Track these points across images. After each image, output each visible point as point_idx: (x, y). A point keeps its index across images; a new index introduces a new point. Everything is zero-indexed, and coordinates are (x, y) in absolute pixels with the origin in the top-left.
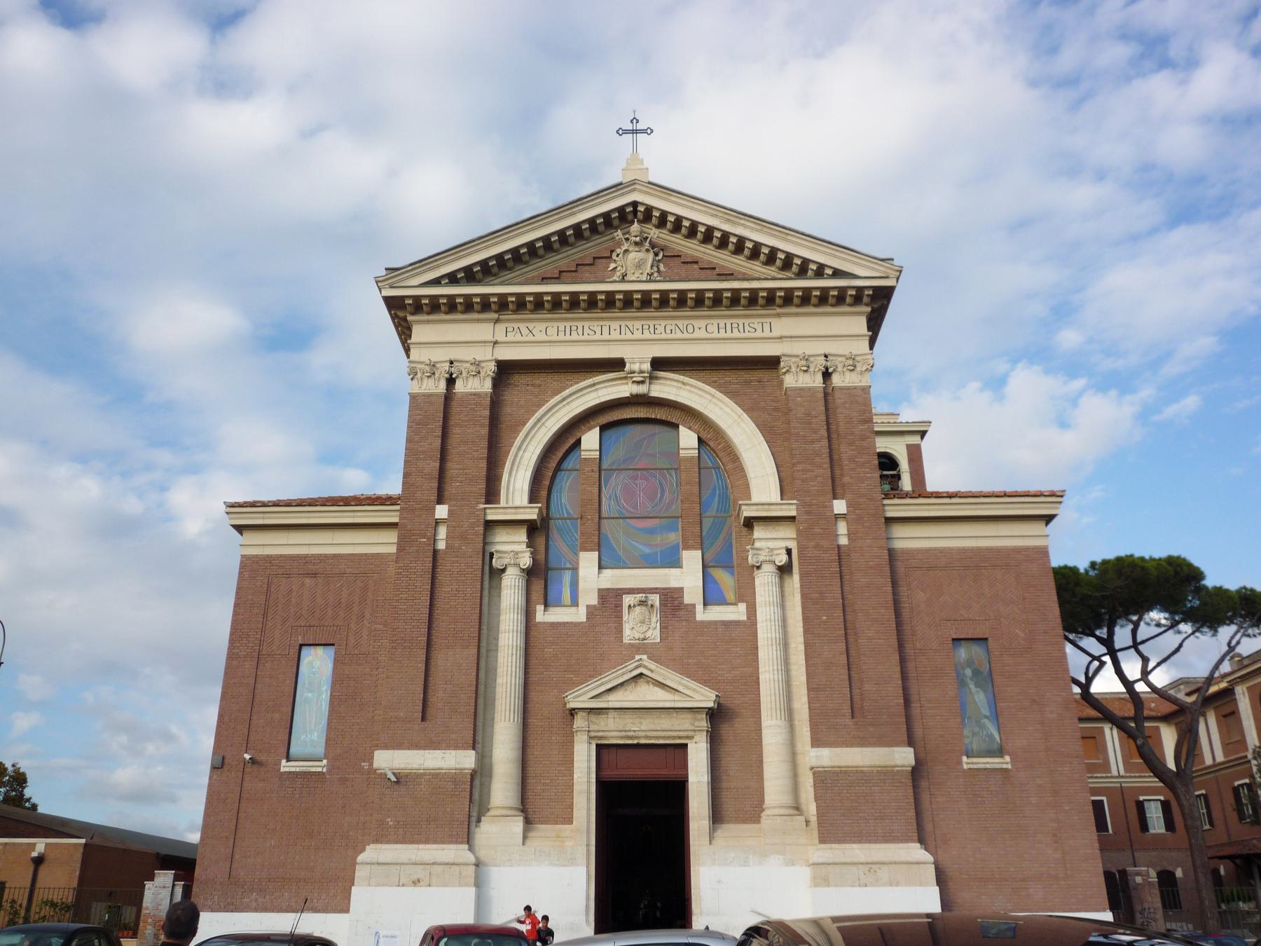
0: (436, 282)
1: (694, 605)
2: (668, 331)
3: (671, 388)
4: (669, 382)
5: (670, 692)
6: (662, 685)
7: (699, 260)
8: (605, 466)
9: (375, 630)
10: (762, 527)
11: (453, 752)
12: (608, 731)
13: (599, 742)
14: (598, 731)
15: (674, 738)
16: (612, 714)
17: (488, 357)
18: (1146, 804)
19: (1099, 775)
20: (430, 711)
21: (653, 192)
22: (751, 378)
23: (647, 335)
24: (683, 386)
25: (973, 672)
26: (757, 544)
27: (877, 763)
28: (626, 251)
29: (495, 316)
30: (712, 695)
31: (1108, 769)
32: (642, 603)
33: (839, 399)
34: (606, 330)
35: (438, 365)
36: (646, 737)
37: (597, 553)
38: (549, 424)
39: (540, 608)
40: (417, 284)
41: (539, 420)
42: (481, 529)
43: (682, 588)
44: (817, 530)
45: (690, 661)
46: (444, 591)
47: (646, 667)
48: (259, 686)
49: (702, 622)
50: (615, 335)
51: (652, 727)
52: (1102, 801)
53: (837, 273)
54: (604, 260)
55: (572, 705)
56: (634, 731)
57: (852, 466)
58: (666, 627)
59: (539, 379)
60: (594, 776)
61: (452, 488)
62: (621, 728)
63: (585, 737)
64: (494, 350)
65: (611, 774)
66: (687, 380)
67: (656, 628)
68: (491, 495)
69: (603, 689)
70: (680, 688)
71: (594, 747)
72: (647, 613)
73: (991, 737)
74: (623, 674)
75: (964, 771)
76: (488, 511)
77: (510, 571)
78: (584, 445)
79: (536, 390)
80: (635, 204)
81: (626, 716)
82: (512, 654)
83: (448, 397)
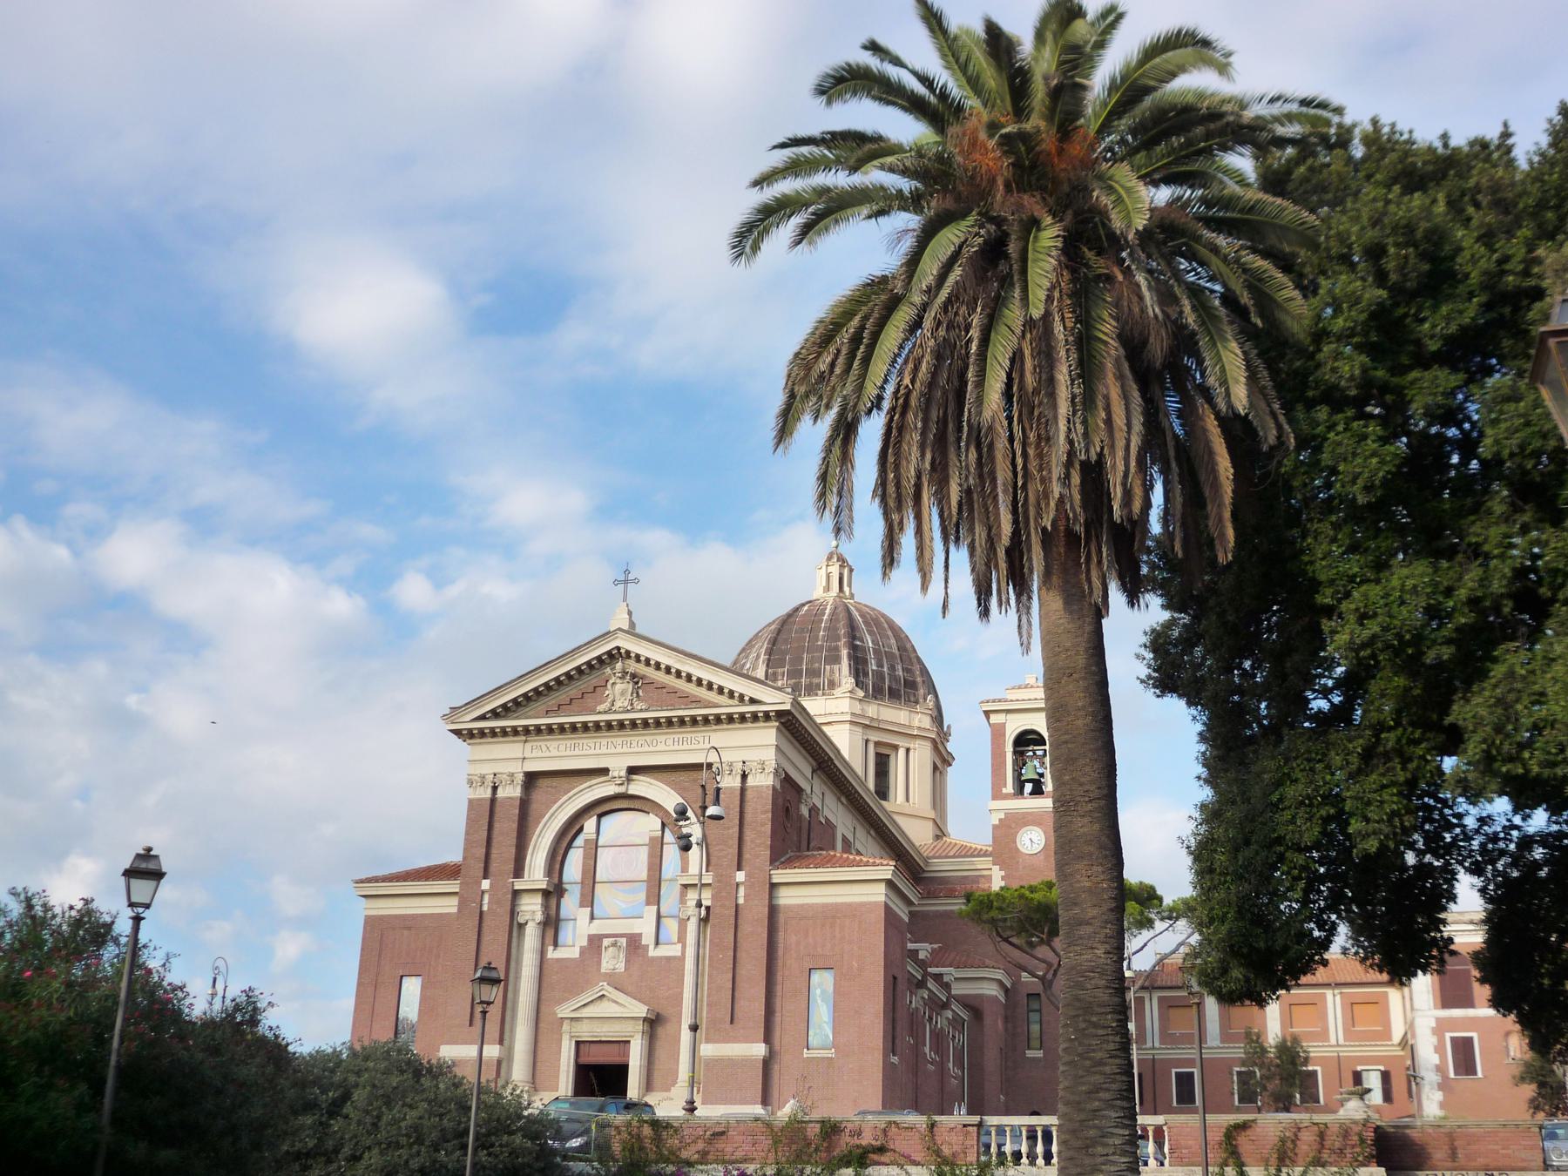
0: (483, 718)
3: (642, 787)
17: (518, 769)
18: (1364, 1074)
19: (1315, 1044)
23: (625, 749)
29: (524, 738)
30: (645, 1009)
31: (1327, 1038)
32: (614, 945)
33: (749, 795)
39: (551, 948)
41: (553, 815)
42: (510, 896)
44: (724, 894)
46: (486, 939)
49: (652, 957)
50: (604, 750)
52: (1316, 1072)
53: (753, 701)
55: (560, 1016)
59: (555, 782)
60: (572, 1061)
61: (493, 867)
65: (584, 1060)
66: (652, 781)
68: (518, 872)
69: (583, 1003)
73: (827, 1036)
77: (530, 924)
79: (553, 790)
80: (618, 648)
83: (493, 800)
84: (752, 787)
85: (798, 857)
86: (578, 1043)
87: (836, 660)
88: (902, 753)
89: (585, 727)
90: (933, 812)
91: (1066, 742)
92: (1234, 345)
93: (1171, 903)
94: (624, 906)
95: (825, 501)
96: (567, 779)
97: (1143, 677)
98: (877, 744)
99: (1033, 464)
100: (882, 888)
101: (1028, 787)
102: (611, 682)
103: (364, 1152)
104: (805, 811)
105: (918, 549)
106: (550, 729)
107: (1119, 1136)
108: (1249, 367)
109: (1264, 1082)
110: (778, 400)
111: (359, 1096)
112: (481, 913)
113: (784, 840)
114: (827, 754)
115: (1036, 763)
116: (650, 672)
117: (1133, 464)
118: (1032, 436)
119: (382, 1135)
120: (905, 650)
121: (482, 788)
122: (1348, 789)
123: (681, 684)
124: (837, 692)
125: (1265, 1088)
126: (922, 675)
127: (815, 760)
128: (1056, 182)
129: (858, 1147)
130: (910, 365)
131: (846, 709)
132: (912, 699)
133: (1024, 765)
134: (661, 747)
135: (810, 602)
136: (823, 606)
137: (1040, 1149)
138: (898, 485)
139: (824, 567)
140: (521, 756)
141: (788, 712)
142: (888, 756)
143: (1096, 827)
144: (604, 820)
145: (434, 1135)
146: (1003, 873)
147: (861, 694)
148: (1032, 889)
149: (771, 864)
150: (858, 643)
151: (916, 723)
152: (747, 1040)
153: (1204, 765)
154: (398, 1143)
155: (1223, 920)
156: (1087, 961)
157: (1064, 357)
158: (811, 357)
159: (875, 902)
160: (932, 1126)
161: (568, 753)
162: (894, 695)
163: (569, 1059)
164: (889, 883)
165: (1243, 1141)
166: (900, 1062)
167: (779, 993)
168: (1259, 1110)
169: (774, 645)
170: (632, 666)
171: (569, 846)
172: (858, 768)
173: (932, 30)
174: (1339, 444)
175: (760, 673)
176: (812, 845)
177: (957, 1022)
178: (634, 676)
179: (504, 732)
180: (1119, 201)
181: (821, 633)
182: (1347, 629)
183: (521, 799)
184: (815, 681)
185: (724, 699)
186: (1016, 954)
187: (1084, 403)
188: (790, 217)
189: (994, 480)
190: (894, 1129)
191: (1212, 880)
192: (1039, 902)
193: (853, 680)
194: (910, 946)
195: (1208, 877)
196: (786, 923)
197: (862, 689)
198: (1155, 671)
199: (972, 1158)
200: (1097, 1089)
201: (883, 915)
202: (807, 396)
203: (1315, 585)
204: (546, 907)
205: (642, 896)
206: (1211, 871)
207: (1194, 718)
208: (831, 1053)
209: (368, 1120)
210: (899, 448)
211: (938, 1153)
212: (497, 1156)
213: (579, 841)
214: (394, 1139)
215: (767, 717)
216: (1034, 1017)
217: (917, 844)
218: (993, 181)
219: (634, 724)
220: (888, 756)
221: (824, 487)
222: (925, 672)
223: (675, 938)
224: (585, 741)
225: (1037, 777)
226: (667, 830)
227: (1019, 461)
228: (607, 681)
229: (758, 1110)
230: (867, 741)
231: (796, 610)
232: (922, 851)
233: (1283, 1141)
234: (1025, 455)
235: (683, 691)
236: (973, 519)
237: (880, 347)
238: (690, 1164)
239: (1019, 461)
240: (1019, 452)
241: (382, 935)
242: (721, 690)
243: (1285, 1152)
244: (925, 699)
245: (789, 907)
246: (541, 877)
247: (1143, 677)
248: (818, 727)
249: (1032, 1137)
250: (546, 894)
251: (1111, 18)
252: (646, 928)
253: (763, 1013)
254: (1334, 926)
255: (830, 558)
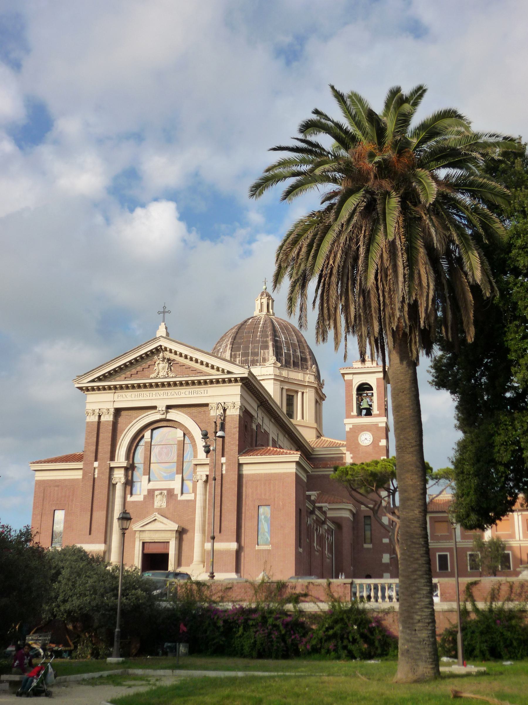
0: (93, 381)
3: (173, 415)
8: (153, 444)
20: (92, 532)
23: (165, 397)
26: (198, 473)
29: (114, 391)
30: (177, 526)
31: (515, 538)
32: (161, 494)
33: (227, 419)
39: (129, 496)
41: (129, 430)
42: (108, 470)
48: (42, 524)
50: (154, 397)
52: (446, 556)
53: (229, 372)
55: (134, 529)
61: (100, 456)
65: (146, 551)
68: (112, 458)
73: (267, 539)
80: (161, 346)
83: (99, 422)
87: (266, 347)
88: (300, 394)
91: (401, 421)
92: (475, 252)
93: (437, 471)
95: (291, 310)
96: (138, 411)
97: (430, 381)
98: (287, 390)
99: (387, 301)
100: (294, 465)
101: (364, 412)
102: (157, 363)
103: (69, 598)
104: (254, 427)
107: (425, 590)
108: (482, 263)
109: (483, 559)
110: (273, 268)
111: (65, 573)
114: (265, 398)
115: (368, 400)
116: (177, 358)
117: (430, 303)
118: (387, 289)
119: (77, 590)
120: (301, 342)
122: (523, 438)
123: (193, 364)
124: (267, 364)
125: (483, 562)
126: (310, 355)
128: (396, 173)
129: (294, 594)
130: (333, 255)
131: (272, 373)
132: (305, 367)
133: (362, 400)
134: (183, 395)
135: (253, 317)
136: (259, 319)
137: (380, 594)
138: (329, 309)
139: (259, 300)
142: (293, 396)
143: (415, 458)
144: (155, 432)
145: (102, 590)
146: (352, 455)
147: (279, 365)
148: (368, 465)
151: (307, 380)
152: (228, 540)
153: (458, 420)
155: (468, 495)
156: (411, 516)
157: (401, 256)
160: (329, 584)
161: (136, 398)
162: (295, 365)
165: (475, 591)
166: (303, 551)
168: (481, 575)
169: (234, 339)
170: (168, 355)
171: (137, 445)
173: (339, 101)
174: (519, 292)
176: (258, 443)
177: (329, 531)
178: (169, 360)
179: (104, 388)
180: (424, 188)
182: (522, 372)
183: (113, 422)
184: (256, 358)
185: (214, 372)
186: (358, 496)
187: (409, 278)
188: (277, 182)
189: (370, 307)
190: (311, 585)
191: (463, 477)
192: (371, 472)
193: (275, 358)
194: (308, 493)
195: (461, 475)
196: (246, 483)
197: (279, 362)
198: (436, 378)
199: (348, 598)
200: (415, 570)
202: (287, 267)
203: (508, 351)
204: (126, 475)
206: (462, 472)
207: (454, 400)
208: (269, 547)
209: (70, 583)
210: (329, 293)
211: (332, 596)
212: (130, 600)
213: (142, 443)
214: (83, 592)
215: (236, 380)
216: (368, 527)
217: (308, 441)
218: (368, 173)
219: (169, 384)
220: (293, 396)
221: (291, 303)
223: (191, 491)
224: (145, 393)
225: (368, 407)
226: (186, 437)
227: (381, 299)
230: (282, 389)
231: (246, 322)
233: (493, 590)
234: (384, 296)
235: (193, 367)
236: (361, 324)
239: (381, 299)
240: (381, 295)
241: (44, 490)
242: (213, 367)
243: (494, 595)
244: (311, 367)
245: (248, 475)
247: (430, 381)
248: (258, 381)
249: (376, 587)
250: (126, 469)
251: (420, 92)
252: (176, 485)
254: (516, 495)
255: (262, 295)
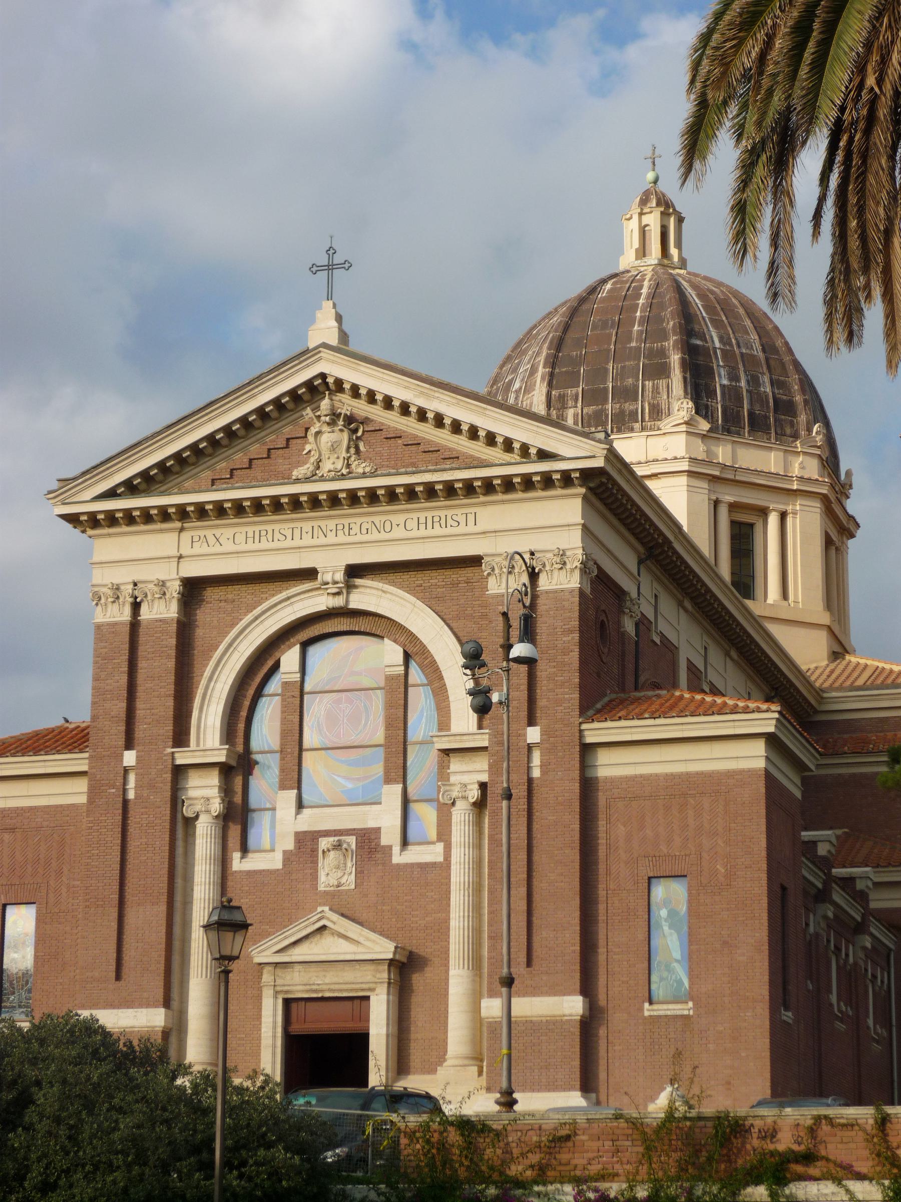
0: (111, 494)
1: (390, 848)
2: (364, 531)
4: (368, 590)
5: (353, 944)
6: (346, 938)
7: (402, 434)
9: (74, 887)
10: (458, 759)
11: (144, 1011)
12: (292, 985)
13: (286, 996)
14: (284, 985)
15: (357, 990)
16: (298, 967)
20: (125, 970)
21: (339, 361)
22: (459, 579)
23: (342, 538)
24: (383, 594)
25: (668, 912)
27: (545, 1013)
28: (318, 433)
29: (178, 524)
32: (338, 846)
33: (543, 605)
34: (297, 532)
35: (122, 587)
36: (330, 990)
37: (295, 791)
38: (242, 648)
39: (237, 855)
40: (88, 498)
41: (230, 645)
42: (168, 776)
43: (379, 829)
45: (384, 908)
47: (328, 919)
50: (307, 540)
51: (335, 980)
53: (544, 455)
54: (299, 441)
55: (257, 960)
56: (318, 985)
57: (551, 686)
58: (362, 872)
59: (232, 592)
60: (279, 1030)
61: (141, 729)
62: (305, 982)
63: (271, 992)
64: (180, 565)
65: (297, 1028)
66: (387, 587)
67: (351, 873)
68: (181, 737)
70: (361, 940)
71: (280, 1002)
72: (342, 857)
73: (680, 982)
74: (306, 927)
75: (645, 1018)
76: (176, 755)
78: (283, 668)
79: (229, 607)
80: (323, 376)
81: (312, 970)
82: (204, 908)
83: (135, 625)
84: (547, 592)
85: (622, 702)
86: (287, 1002)
88: (773, 520)
89: (276, 505)
90: (828, 614)
94: (350, 785)
98: (733, 507)
100: (759, 748)
102: (313, 430)
103: (59, 1177)
104: (629, 626)
105: (887, 317)
106: (220, 510)
112: (125, 802)
113: (599, 675)
116: (376, 413)
120: (775, 350)
121: (116, 605)
123: (427, 431)
124: (666, 424)
126: (803, 391)
127: (643, 544)
129: (772, 1154)
130: (875, 58)
131: (681, 452)
132: (788, 431)
135: (615, 275)
136: (635, 283)
138: (864, 239)
140: (174, 552)
141: (600, 472)
142: (751, 526)
149: (581, 715)
150: (699, 342)
151: (796, 471)
154: (110, 1164)
158: (729, 45)
159: (749, 770)
162: (758, 425)
163: (275, 1028)
164: (771, 740)
167: (602, 917)
170: (347, 404)
171: (259, 694)
172: (703, 543)
175: (539, 406)
176: (642, 679)
178: (350, 419)
179: (147, 516)
181: (636, 328)
184: (628, 407)
185: (496, 454)
190: (825, 1128)
193: (691, 404)
194: (806, 835)
196: (608, 806)
197: (706, 417)
201: (763, 790)
202: (725, 103)
204: (226, 791)
205: (378, 769)
208: (686, 1009)
210: (864, 182)
212: (250, 1179)
213: (274, 686)
215: (567, 479)
217: (804, 668)
219: (353, 498)
221: (743, 221)
222: (807, 385)
223: (433, 834)
224: (277, 527)
228: (307, 429)
229: (575, 1099)
230: (716, 503)
231: (593, 290)
232: (813, 678)
235: (429, 442)
237: (838, 44)
238: (519, 1184)
242: (491, 439)
244: (809, 430)
245: (612, 780)
246: (216, 743)
248: (638, 482)
250: (226, 770)
253: (578, 948)
255: (644, 202)
